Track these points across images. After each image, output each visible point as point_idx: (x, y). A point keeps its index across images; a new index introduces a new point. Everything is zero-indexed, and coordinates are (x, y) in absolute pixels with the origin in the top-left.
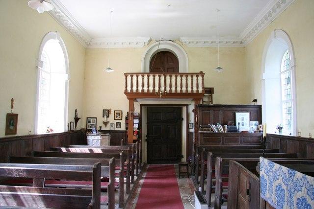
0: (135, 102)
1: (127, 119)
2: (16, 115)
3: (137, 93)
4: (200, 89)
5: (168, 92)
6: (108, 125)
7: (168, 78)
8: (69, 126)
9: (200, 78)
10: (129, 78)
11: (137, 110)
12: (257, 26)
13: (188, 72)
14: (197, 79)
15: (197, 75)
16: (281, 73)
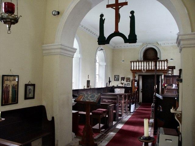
1: (132, 81)
4: (166, 68)
6: (124, 85)
10: (132, 63)
11: (137, 78)
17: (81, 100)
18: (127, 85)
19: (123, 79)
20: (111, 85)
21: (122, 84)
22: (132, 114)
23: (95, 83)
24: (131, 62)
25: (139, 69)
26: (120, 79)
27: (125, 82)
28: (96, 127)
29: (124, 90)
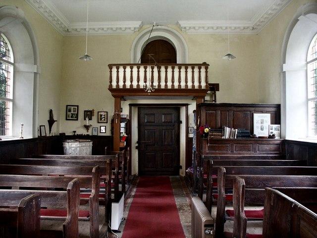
0: (122, 102)
1: (113, 121)
3: (125, 89)
4: (203, 84)
5: (157, 87)
6: (90, 130)
7: (149, 69)
8: (39, 131)
9: (203, 70)
13: (188, 63)
14: (145, 72)
15: (200, 66)
16: (307, 63)
19: (89, 114)
20: (56, 130)
21: (87, 127)
24: (111, 66)
25: (131, 86)
26: (81, 115)
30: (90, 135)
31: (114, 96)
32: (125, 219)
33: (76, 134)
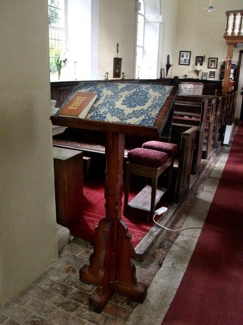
1: (223, 67)
2: (120, 59)
3: (233, 37)
6: (200, 74)
12: (46, 309)
17: (82, 116)
18: (210, 75)
19: (200, 60)
20: (172, 74)
22: (228, 149)
23: (133, 69)
24: (228, 14)
27: (204, 69)
28: (142, 200)
29: (201, 87)
30: (200, 79)
31: (229, 44)
32: (193, 173)
33: (187, 77)
